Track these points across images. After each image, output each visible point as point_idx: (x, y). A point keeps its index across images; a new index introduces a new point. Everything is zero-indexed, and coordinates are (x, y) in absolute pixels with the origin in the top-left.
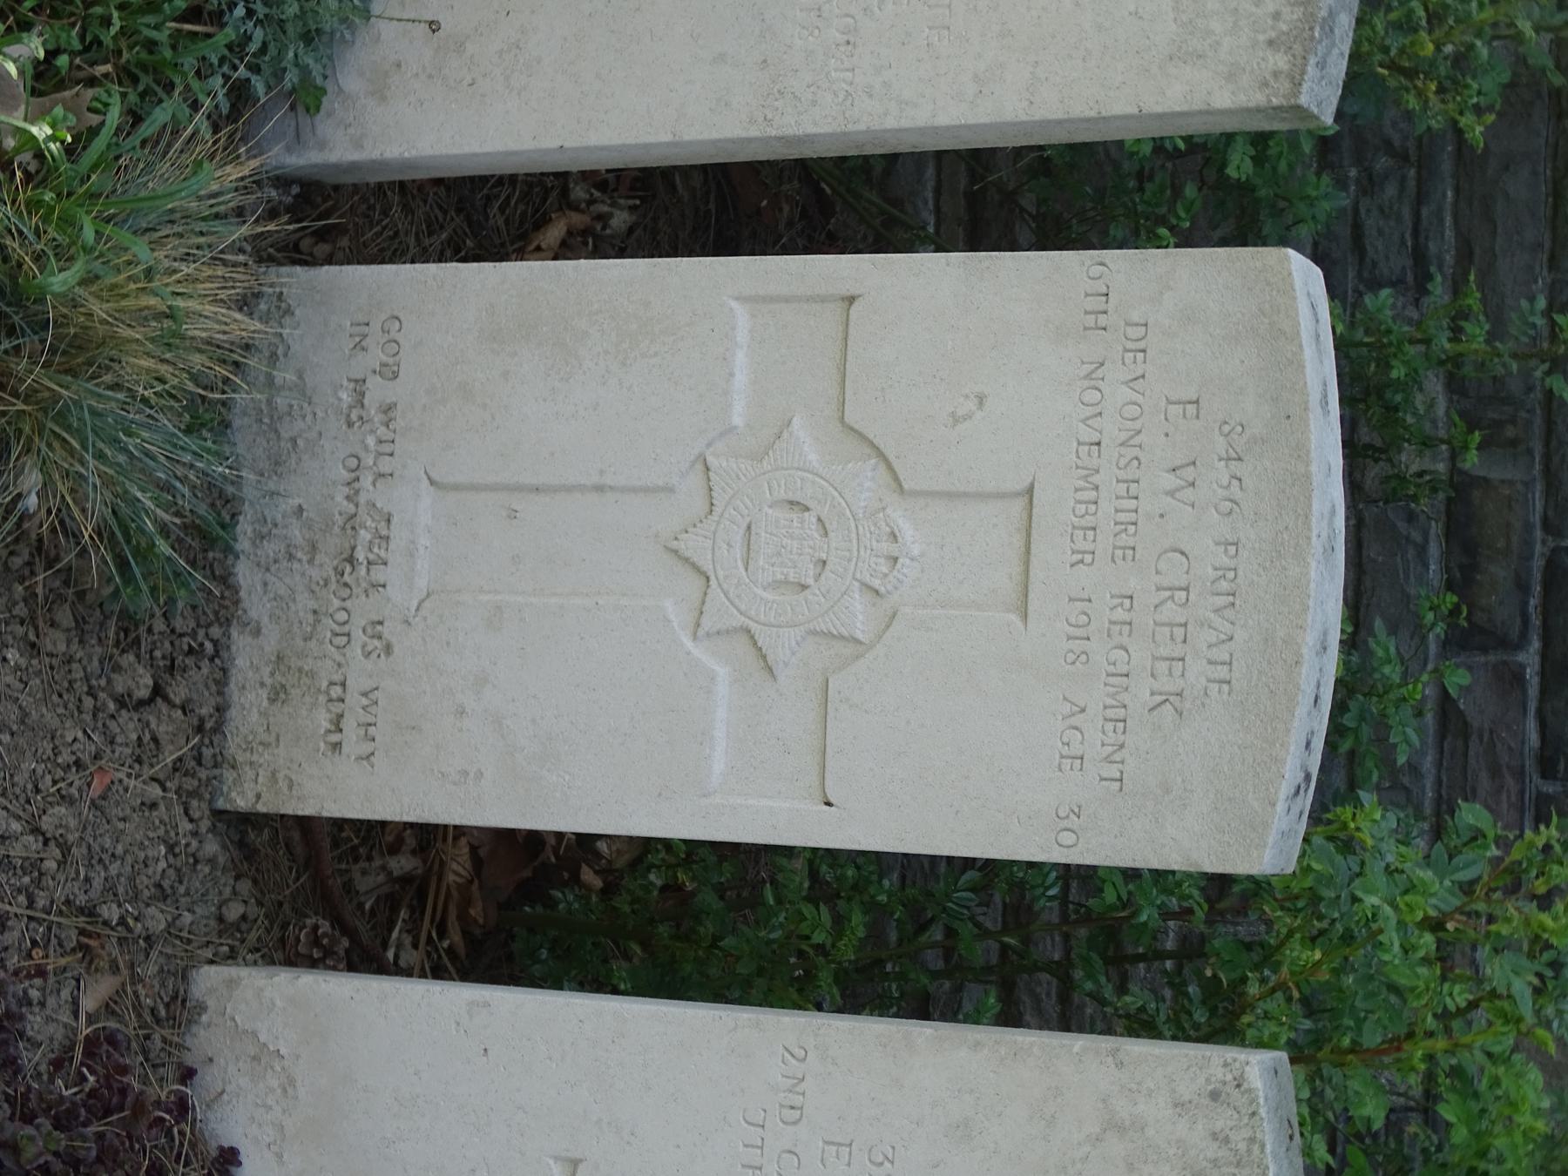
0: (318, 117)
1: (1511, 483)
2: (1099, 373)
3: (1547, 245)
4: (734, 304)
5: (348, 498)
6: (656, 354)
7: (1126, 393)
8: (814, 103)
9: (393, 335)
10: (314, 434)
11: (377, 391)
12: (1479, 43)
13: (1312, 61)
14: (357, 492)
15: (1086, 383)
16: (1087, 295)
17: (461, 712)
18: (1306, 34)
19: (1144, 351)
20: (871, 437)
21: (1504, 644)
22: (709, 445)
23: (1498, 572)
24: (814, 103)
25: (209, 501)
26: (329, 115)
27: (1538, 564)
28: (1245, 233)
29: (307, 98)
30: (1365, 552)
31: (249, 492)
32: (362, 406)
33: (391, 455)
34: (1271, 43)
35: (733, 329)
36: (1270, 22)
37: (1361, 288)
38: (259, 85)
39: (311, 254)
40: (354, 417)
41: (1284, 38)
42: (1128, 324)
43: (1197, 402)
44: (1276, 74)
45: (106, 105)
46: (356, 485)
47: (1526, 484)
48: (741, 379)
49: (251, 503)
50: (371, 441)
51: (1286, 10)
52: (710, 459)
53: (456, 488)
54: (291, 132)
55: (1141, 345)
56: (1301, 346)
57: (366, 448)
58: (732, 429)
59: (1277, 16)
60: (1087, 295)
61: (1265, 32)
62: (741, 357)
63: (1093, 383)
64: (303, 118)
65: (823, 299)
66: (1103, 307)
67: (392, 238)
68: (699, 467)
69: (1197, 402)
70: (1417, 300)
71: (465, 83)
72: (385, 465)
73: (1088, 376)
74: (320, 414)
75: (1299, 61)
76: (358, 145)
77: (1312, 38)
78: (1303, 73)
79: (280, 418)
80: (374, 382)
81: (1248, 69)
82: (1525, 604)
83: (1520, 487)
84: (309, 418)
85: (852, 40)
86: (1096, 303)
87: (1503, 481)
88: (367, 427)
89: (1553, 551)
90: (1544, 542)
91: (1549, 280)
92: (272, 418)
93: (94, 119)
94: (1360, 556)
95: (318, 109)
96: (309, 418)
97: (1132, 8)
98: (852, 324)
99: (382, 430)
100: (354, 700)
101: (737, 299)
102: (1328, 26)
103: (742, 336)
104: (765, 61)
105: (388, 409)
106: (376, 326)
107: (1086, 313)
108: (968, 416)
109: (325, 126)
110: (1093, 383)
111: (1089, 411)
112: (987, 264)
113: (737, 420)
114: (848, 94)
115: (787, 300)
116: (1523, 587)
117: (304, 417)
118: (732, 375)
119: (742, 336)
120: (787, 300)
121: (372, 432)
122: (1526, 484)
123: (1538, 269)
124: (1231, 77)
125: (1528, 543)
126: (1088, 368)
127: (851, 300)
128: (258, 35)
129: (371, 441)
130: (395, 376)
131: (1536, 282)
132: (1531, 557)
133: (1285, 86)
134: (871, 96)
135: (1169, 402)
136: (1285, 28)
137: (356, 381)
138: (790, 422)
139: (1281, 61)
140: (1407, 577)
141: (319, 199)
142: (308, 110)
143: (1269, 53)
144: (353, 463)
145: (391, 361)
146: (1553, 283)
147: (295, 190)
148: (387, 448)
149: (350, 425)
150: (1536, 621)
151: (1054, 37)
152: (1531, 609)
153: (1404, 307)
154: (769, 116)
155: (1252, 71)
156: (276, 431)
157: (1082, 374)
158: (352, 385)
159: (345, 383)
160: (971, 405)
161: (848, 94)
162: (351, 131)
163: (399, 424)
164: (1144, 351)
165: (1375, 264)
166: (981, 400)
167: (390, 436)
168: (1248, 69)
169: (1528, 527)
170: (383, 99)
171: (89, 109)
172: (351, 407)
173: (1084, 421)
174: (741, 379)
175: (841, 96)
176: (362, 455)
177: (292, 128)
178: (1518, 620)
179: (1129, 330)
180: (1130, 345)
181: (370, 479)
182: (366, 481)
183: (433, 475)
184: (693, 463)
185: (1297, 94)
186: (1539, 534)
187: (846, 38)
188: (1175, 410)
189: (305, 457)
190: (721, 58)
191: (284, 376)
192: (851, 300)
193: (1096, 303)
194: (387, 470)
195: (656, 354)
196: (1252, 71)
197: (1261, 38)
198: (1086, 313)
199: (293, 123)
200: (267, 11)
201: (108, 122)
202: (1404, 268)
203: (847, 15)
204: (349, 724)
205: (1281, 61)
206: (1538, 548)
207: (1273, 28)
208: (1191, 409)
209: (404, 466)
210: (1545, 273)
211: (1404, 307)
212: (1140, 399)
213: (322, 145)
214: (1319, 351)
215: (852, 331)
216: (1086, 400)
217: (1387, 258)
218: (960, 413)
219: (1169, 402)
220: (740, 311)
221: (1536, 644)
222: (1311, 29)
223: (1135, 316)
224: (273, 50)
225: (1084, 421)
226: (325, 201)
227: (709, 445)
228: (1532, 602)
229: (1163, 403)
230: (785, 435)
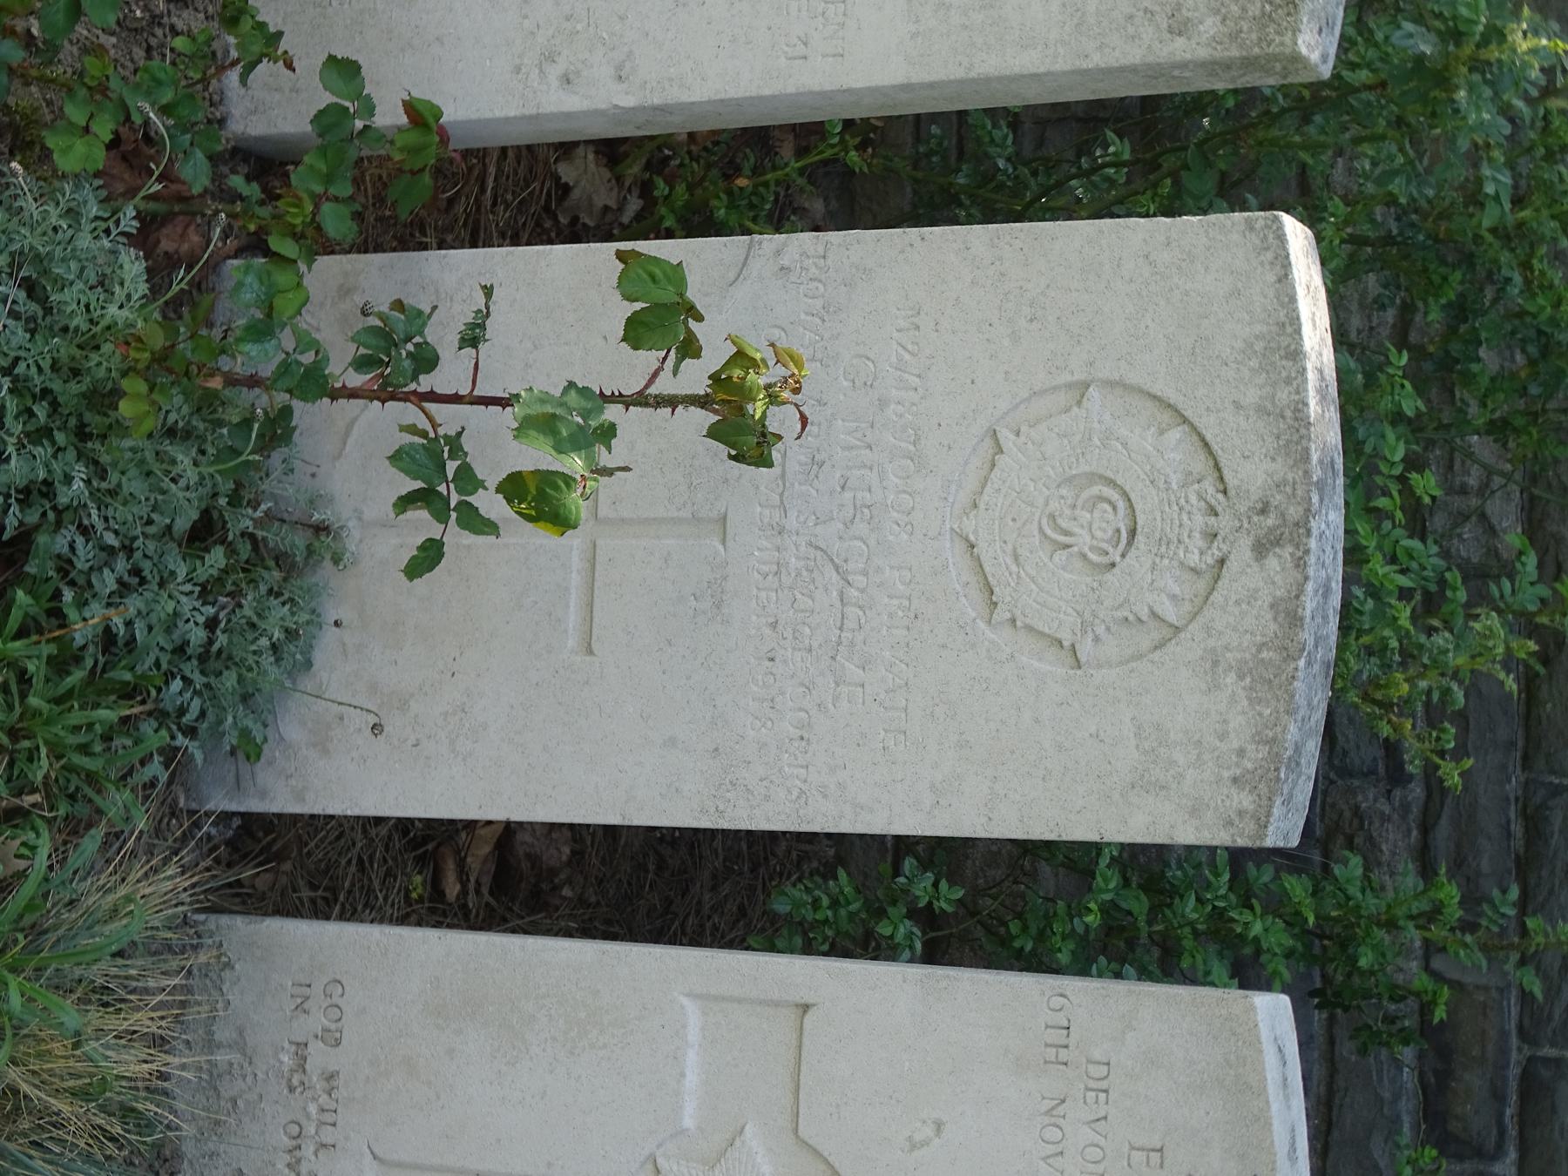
0: (259, 765)
1: (1486, 989)
2: (1061, 1110)
3: (1520, 744)
4: (685, 1001)
5: (289, 1165)
6: (605, 1046)
7: (1087, 1134)
8: (767, 798)
9: (336, 999)
10: (253, 1097)
11: (319, 1057)
12: (1455, 686)
13: (1278, 802)
14: (299, 1161)
15: (1047, 1120)
16: (1047, 1027)
18: (1272, 775)
19: (1106, 1091)
20: (826, 1154)
21: (1480, 1153)
22: (659, 1146)
23: (1472, 1080)
24: (767, 798)
25: (145, 1165)
26: (270, 763)
27: (1514, 1072)
28: (1231, 194)
29: (249, 750)
30: (1337, 1048)
31: (188, 1148)
32: (304, 1071)
33: (334, 1125)
34: (1235, 780)
35: (684, 1027)
36: (1234, 758)
37: (1332, 775)
38: (195, 749)
39: (253, 887)
40: (295, 1082)
41: (1248, 776)
42: (1089, 1061)
43: (1161, 1150)
44: (1241, 813)
45: (33, 848)
46: (297, 1153)
47: (1501, 990)
48: (692, 1079)
49: (191, 1162)
50: (313, 1109)
51: (1251, 747)
52: (659, 1160)
53: (400, 1165)
54: (231, 778)
55: (1104, 1084)
56: (1267, 1102)
57: (308, 1116)
58: (683, 1131)
59: (1241, 752)
60: (1047, 1027)
61: (1229, 768)
62: (692, 1057)
63: (1053, 1120)
64: (244, 767)
65: (777, 1004)
66: (1064, 1041)
67: (338, 838)
68: (650, 1166)
69: (1161, 1150)
70: (1389, 792)
71: (410, 743)
72: (328, 1135)
73: (1049, 1112)
74: (260, 1075)
75: (1265, 802)
76: (300, 798)
77: (1278, 779)
78: (1269, 814)
79: (219, 1076)
80: (316, 1049)
81: (1212, 804)
82: (1501, 1115)
83: (1494, 994)
84: (249, 1079)
85: (806, 736)
86: (1058, 1036)
87: (1477, 987)
88: (309, 1094)
89: (1530, 1059)
90: (1520, 1050)
91: (1522, 779)
92: (211, 1075)
93: (21, 864)
94: (1332, 1052)
95: (258, 757)
96: (249, 1079)
97: (1093, 729)
98: (806, 1033)
99: (324, 1099)
101: (688, 995)
102: (1294, 763)
103: (693, 1034)
104: (716, 749)
105: (331, 1077)
106: (318, 989)
107: (1047, 1045)
108: (925, 1143)
109: (264, 775)
110: (1053, 1120)
111: (1051, 1149)
112: (944, 984)
113: (688, 1122)
114: (802, 792)
115: (739, 1001)
116: (1499, 1097)
117: (244, 1077)
118: (683, 1075)
119: (693, 1034)
120: (739, 1001)
121: (314, 1099)
122: (1501, 990)
123: (1511, 769)
124: (1194, 812)
125: (1504, 1051)
126: (1048, 1104)
127: (806, 1008)
128: (196, 705)
129: (313, 1109)
130: (338, 1043)
131: (1510, 782)
132: (1506, 1066)
133: (1251, 827)
134: (825, 796)
135: (1132, 1148)
136: (1250, 766)
137: (298, 1044)
138: (743, 1128)
139: (1246, 800)
140: (1380, 1079)
141: (261, 834)
142: (248, 758)
143: (1234, 791)
144: (295, 1130)
145: (333, 1026)
146: (1527, 783)
147: (236, 822)
148: (329, 1118)
149: (292, 1089)
150: (1512, 1131)
151: (1013, 752)
152: (1507, 1119)
153: (1375, 800)
154: (721, 808)
155: (1216, 808)
156: (216, 1089)
157: (1044, 1109)
158: (293, 1048)
159: (286, 1045)
160: (929, 1131)
161: (802, 792)
162: (293, 782)
163: (341, 1093)
164: (1106, 1091)
165: (1345, 753)
166: (939, 1126)
167: (333, 1106)
168: (1212, 804)
169: (1504, 1034)
170: (325, 752)
171: (16, 856)
172: (292, 1071)
173: (1044, 1159)
174: (692, 1079)
175: (795, 793)
176: (304, 1122)
177: (232, 774)
178: (1495, 1132)
179: (1091, 1068)
180: (1092, 1084)
181: (312, 1149)
182: (308, 1150)
183: (376, 1150)
184: (643, 1164)
185: (1263, 837)
186: (1514, 1041)
187: (799, 732)
188: (1138, 1156)
189: (246, 1119)
190: (672, 742)
191: (223, 1034)
192: (806, 1008)
193: (1058, 1036)
194: (329, 1141)
195: (605, 1046)
196: (1216, 808)
197: (1226, 774)
198: (1047, 1045)
199: (233, 768)
200: (205, 680)
201: (36, 867)
202: (1375, 759)
203: (801, 709)
205: (1246, 800)
206: (1514, 1056)
207: (1237, 765)
208: (1155, 1157)
209: (347, 1138)
210: (1519, 771)
211: (1375, 800)
212: (1102, 1142)
213: (263, 794)
214: (1287, 1098)
215: (806, 1041)
216: (1047, 1136)
217: (1358, 747)
218: (918, 1137)
219: (1132, 1148)
220: (692, 1009)
221: (1513, 1155)
222: (1277, 769)
223: (1097, 1054)
224: (211, 716)
225: (1044, 1159)
226: (266, 835)
227: (659, 1146)
228: (1508, 1112)
229: (1126, 1149)
230: (738, 1143)
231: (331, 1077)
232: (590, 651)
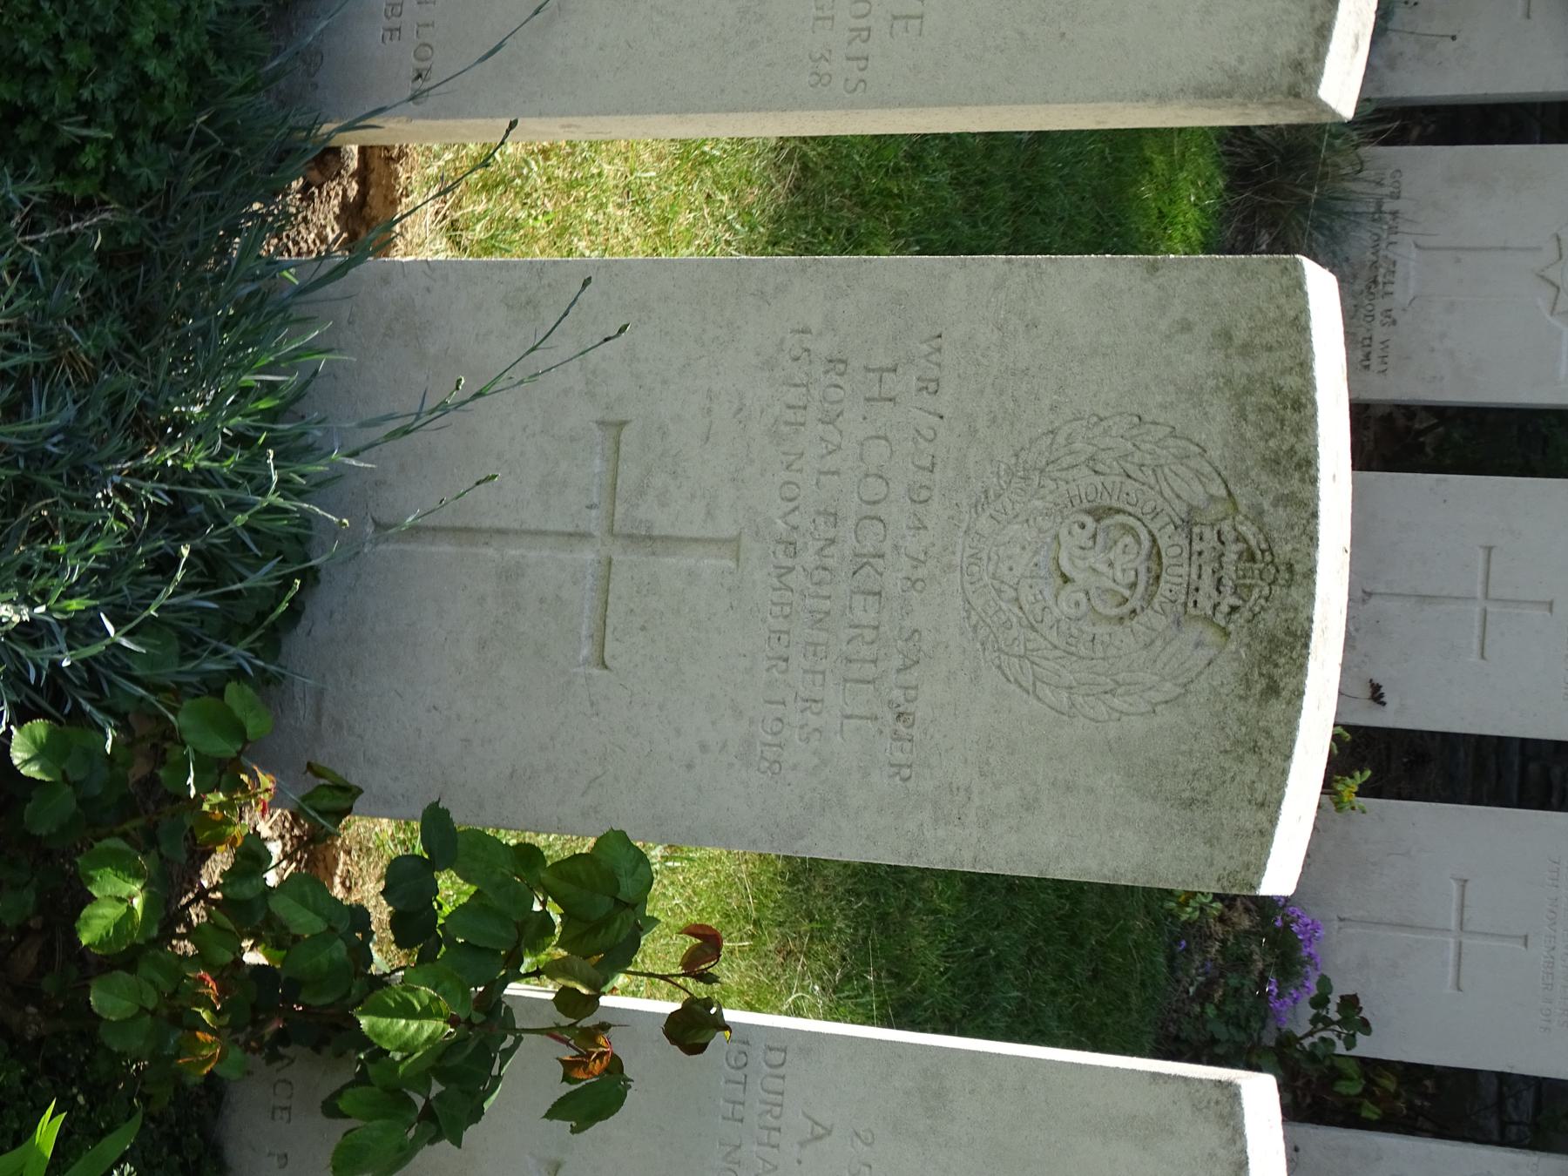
17: (1433, 350)
53: (1429, 249)
100: (1376, 346)
204: (1374, 357)
231: (1395, 214)
232: (1528, 17)
